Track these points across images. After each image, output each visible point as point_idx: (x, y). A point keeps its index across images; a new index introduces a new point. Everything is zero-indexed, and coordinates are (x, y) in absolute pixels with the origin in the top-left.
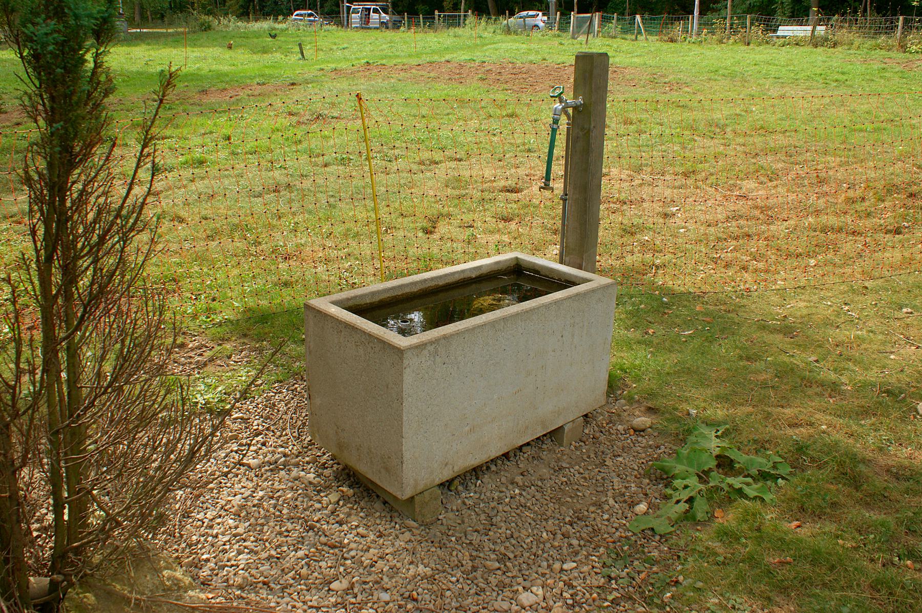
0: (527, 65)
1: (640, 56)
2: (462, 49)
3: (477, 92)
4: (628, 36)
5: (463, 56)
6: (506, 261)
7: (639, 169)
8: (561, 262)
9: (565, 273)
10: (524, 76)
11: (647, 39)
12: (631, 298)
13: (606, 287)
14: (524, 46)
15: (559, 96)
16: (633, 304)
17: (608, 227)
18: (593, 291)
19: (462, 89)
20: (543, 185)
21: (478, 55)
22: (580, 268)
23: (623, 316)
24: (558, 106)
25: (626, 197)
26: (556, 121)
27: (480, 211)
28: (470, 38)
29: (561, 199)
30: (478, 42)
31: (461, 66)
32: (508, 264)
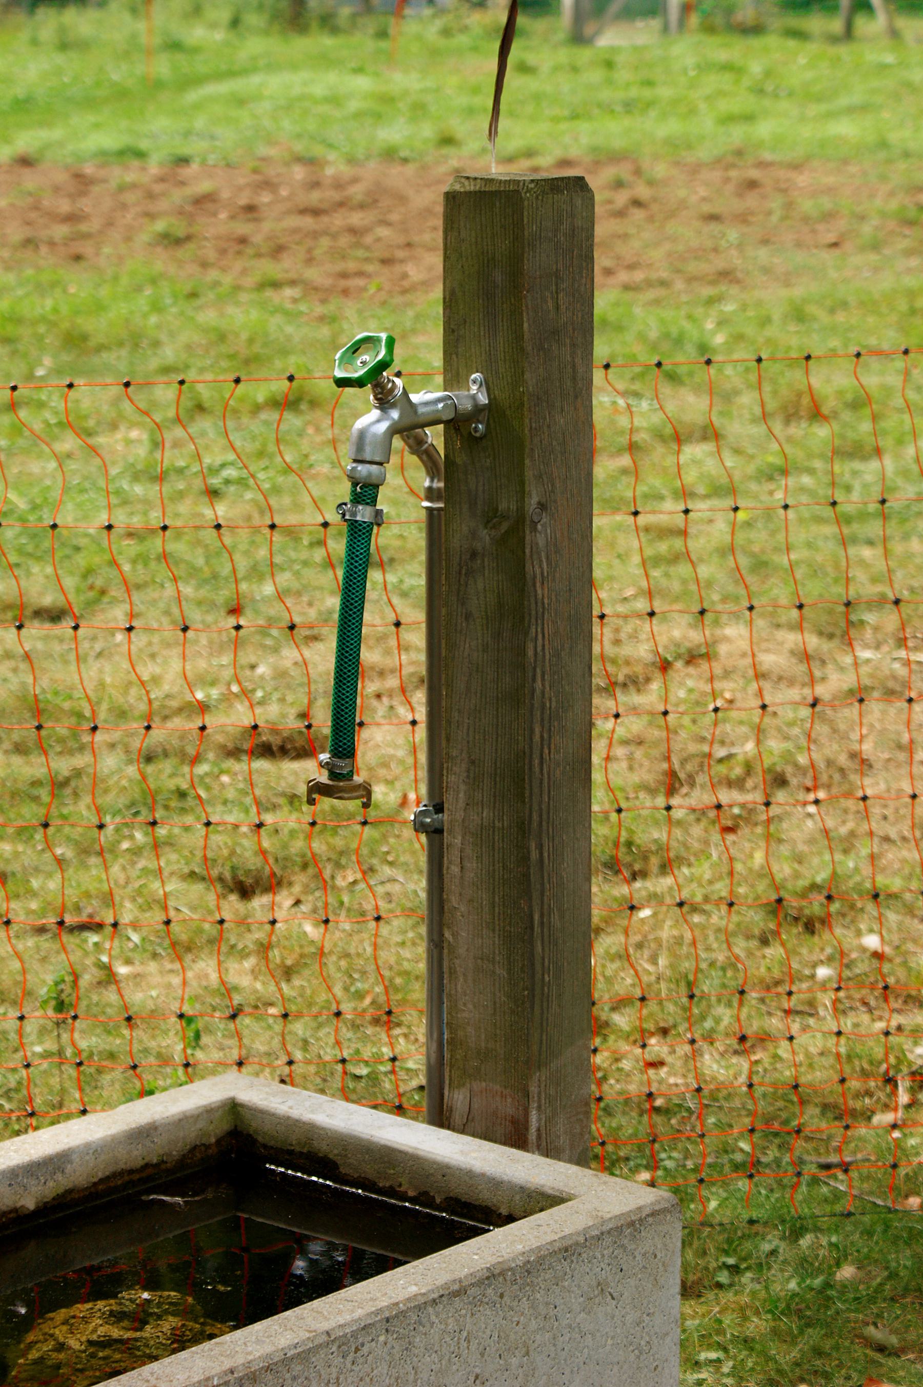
0: (371, 170)
1: (863, 109)
2: (89, 103)
3: (142, 302)
4: (816, 23)
5: (91, 137)
6: (183, 1120)
7: (844, 622)
8: (440, 1117)
9: (444, 1170)
10: (356, 219)
11: (894, 34)
12: (796, 1233)
13: (633, 1225)
14: (363, 83)
15: (375, 378)
16: (805, 1266)
17: (632, 947)
18: (568, 1251)
19: (79, 285)
20: (323, 778)
21: (160, 131)
22: (516, 1137)
23: (758, 1325)
24: (372, 421)
25: (788, 757)
26: (365, 491)
27: (136, 852)
28: (131, 49)
29: (419, 826)
30: (162, 67)
31: (82, 182)
32: (191, 1135)
